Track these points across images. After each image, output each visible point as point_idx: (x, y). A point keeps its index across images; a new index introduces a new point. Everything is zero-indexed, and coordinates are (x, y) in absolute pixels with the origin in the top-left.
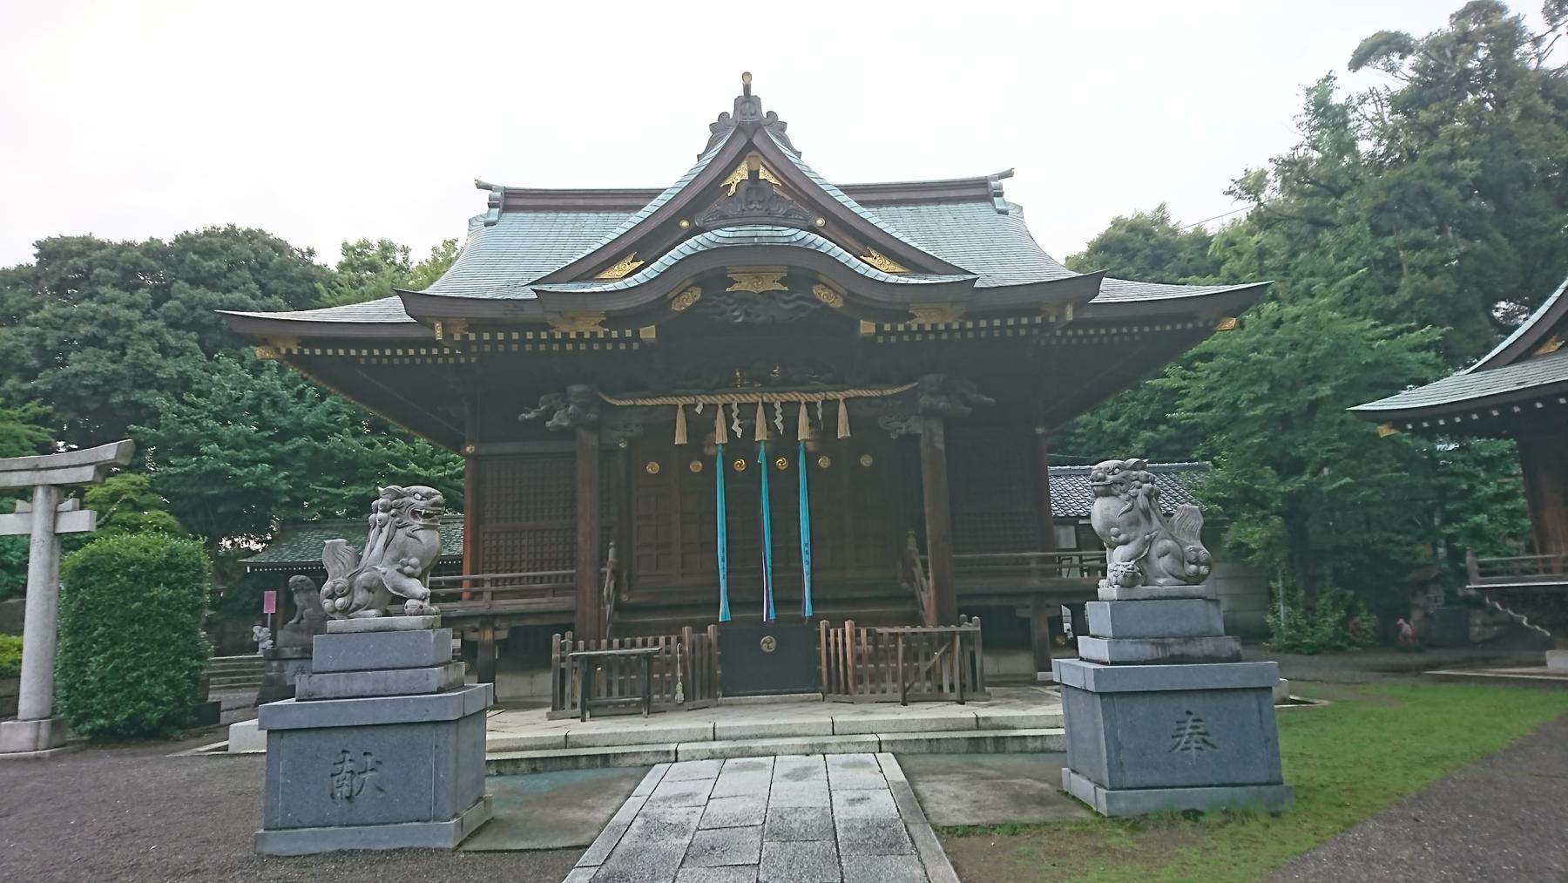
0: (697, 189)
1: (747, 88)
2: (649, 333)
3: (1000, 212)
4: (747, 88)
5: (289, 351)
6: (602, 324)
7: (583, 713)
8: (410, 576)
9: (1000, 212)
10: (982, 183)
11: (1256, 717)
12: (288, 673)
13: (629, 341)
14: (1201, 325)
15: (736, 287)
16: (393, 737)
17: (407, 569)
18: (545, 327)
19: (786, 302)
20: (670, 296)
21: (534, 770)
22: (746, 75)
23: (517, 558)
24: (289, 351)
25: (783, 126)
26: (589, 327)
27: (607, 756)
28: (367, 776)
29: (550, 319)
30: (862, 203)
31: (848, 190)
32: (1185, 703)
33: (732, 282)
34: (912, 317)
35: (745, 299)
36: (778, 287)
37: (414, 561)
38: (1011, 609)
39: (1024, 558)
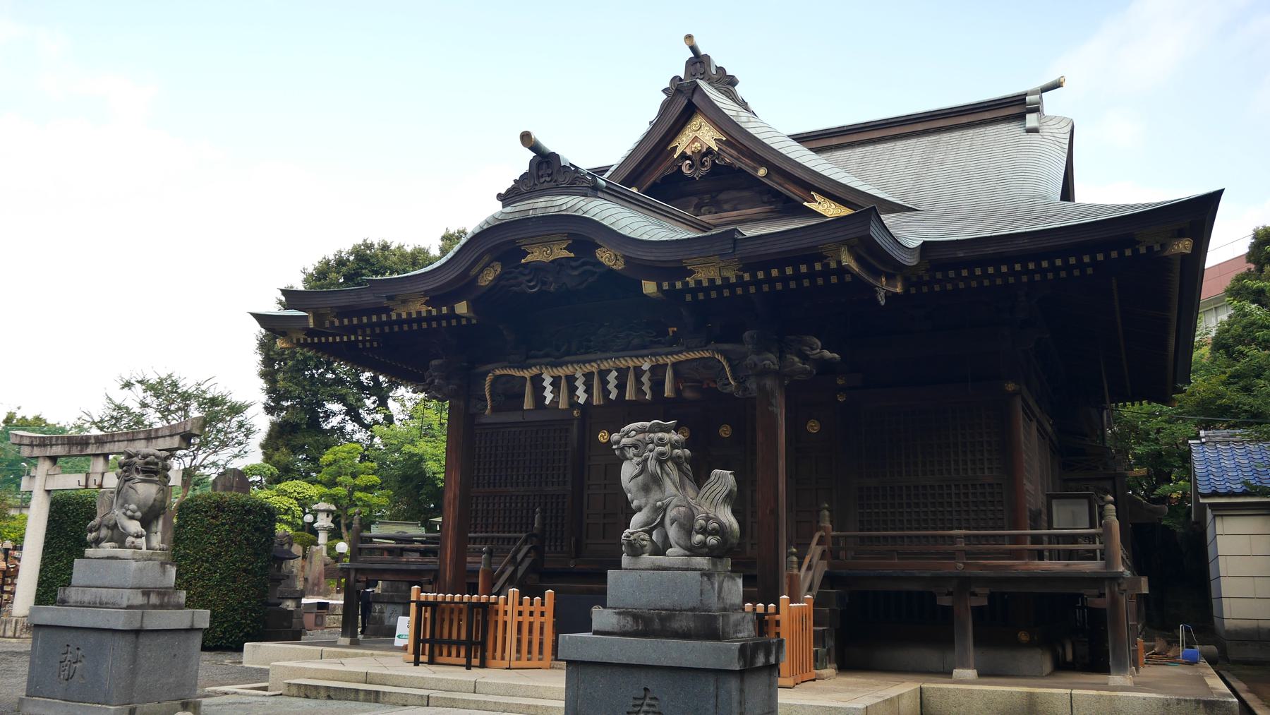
0: (641, 156)
1: (693, 49)
2: (462, 308)
3: (1029, 131)
4: (693, 49)
5: (298, 340)
6: (427, 303)
7: (468, 657)
8: (132, 518)
9: (1029, 131)
10: (1019, 100)
11: (712, 701)
12: (386, 615)
13: (446, 317)
14: (1143, 250)
15: (529, 258)
16: (93, 638)
17: (129, 513)
18: (387, 310)
19: (574, 268)
20: (473, 272)
21: (329, 697)
22: (689, 37)
23: (490, 520)
24: (298, 340)
25: (732, 81)
26: (419, 307)
27: (377, 692)
28: (78, 665)
29: (391, 304)
30: (817, 150)
31: (801, 139)
32: (644, 680)
33: (525, 254)
34: (691, 273)
35: (538, 267)
36: (565, 254)
37: (133, 506)
38: (933, 596)
39: (951, 537)
